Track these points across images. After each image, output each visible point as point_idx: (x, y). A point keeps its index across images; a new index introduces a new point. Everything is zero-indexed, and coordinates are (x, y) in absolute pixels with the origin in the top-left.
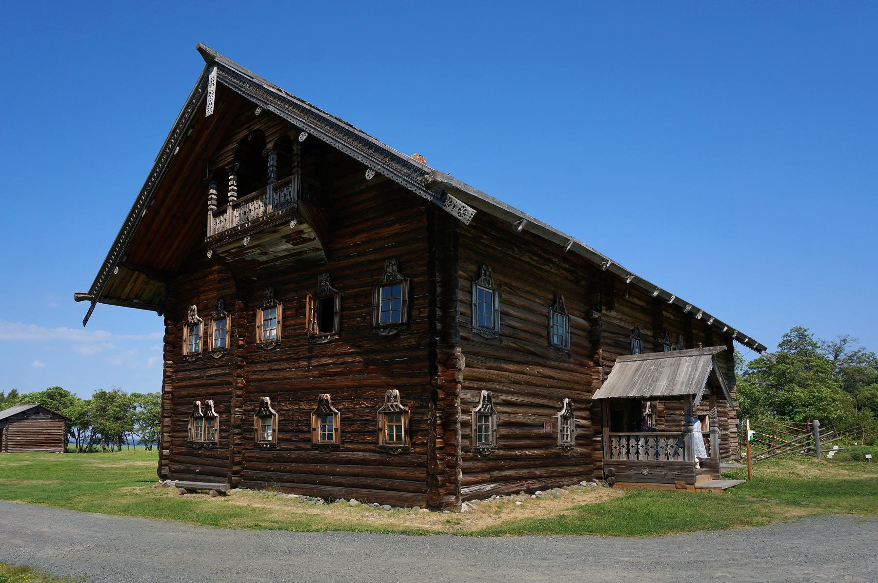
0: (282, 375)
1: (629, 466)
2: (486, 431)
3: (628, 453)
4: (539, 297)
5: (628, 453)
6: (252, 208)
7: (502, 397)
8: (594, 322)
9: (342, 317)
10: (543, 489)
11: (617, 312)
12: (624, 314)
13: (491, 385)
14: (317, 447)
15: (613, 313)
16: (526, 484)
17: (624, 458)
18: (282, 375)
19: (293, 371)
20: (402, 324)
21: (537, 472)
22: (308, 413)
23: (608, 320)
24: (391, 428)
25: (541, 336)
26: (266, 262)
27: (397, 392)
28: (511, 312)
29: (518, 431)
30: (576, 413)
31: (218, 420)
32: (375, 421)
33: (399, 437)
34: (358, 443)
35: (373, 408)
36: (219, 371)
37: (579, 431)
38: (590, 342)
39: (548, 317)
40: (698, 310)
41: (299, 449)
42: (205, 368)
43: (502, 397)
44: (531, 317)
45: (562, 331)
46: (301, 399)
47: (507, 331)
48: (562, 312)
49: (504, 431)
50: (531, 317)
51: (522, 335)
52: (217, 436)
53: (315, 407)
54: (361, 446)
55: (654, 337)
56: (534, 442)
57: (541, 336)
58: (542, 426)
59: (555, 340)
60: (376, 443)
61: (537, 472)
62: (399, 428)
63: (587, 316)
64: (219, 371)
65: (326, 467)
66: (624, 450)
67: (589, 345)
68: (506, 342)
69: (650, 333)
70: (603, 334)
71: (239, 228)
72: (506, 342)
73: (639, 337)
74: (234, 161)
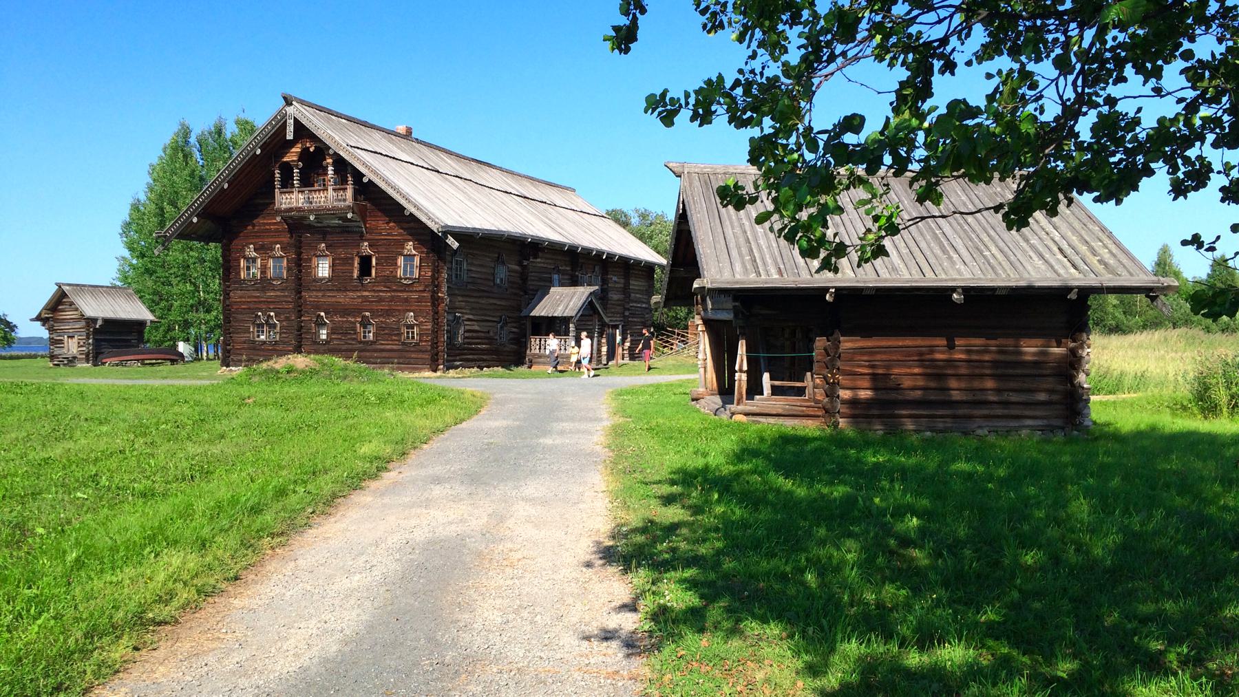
0: (334, 300)
1: (540, 357)
2: (460, 271)
3: (540, 349)
4: (489, 257)
5: (540, 349)
6: (315, 196)
7: (467, 316)
8: (524, 267)
9: (376, 269)
10: (488, 367)
11: (541, 258)
12: (547, 259)
13: (460, 310)
14: (361, 342)
15: (539, 260)
16: (478, 363)
17: (537, 351)
18: (334, 300)
19: (343, 298)
20: (415, 279)
21: (485, 357)
22: (354, 323)
23: (534, 265)
24: (408, 333)
25: (489, 280)
26: (320, 227)
27: (412, 314)
28: (473, 269)
29: (474, 335)
30: (509, 325)
31: (279, 326)
32: (399, 329)
33: (413, 337)
34: (388, 340)
35: (398, 322)
36: (279, 293)
37: (512, 336)
38: (522, 280)
39: (494, 268)
40: (604, 253)
41: (347, 343)
42: (264, 289)
43: (467, 316)
44: (484, 270)
45: (503, 276)
46: (349, 315)
47: (470, 280)
48: (503, 263)
49: (466, 335)
50: (484, 270)
51: (479, 281)
52: (278, 336)
53: (360, 320)
54: (391, 342)
55: (572, 270)
56: (484, 341)
57: (489, 280)
58: (489, 332)
59: (498, 281)
60: (399, 341)
61: (485, 357)
62: (413, 333)
63: (520, 264)
64: (279, 293)
65: (368, 354)
66: (538, 347)
67: (520, 282)
68: (469, 287)
69: (568, 268)
70: (530, 274)
71: (312, 218)
72: (469, 287)
73: (559, 272)
74: (299, 161)
